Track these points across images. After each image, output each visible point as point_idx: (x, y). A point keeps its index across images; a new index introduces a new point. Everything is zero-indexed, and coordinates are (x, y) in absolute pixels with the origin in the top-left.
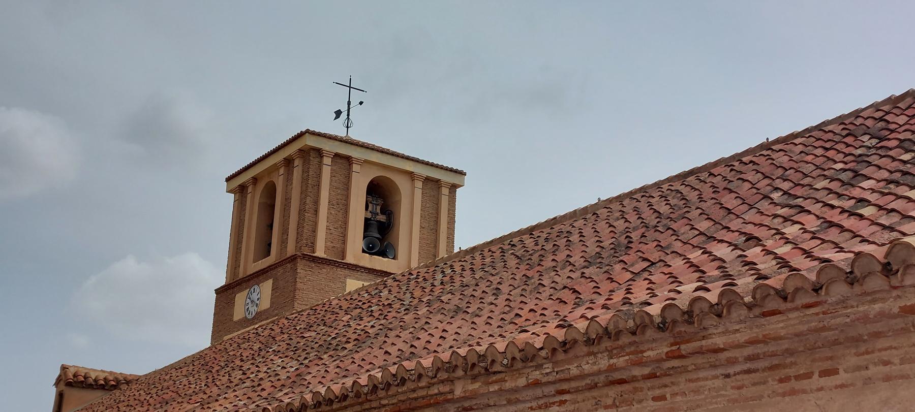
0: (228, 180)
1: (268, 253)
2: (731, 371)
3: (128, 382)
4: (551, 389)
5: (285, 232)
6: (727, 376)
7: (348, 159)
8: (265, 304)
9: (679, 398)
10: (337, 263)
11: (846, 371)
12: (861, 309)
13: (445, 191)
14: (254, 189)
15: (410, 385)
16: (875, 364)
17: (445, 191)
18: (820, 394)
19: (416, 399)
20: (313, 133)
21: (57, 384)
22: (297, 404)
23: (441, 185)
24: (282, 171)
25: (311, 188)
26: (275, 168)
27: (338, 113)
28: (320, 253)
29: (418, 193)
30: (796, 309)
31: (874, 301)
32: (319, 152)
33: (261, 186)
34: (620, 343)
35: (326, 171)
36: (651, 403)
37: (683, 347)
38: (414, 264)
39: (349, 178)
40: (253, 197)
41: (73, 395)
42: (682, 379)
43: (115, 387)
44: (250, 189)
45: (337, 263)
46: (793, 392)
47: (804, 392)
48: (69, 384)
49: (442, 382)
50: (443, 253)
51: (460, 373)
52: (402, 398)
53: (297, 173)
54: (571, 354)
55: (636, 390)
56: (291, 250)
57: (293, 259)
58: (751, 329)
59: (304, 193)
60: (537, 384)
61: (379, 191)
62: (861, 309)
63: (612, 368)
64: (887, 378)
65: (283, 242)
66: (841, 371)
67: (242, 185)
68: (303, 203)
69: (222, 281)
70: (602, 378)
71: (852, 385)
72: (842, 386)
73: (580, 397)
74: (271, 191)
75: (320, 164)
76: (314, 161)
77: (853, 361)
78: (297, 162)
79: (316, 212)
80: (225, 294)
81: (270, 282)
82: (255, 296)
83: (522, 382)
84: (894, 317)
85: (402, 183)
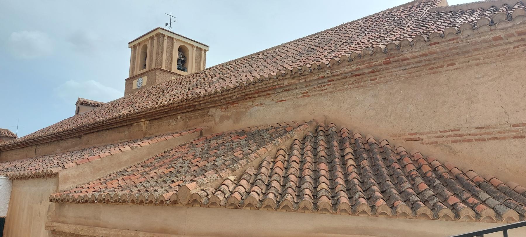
0: (129, 43)
1: (145, 68)
2: (407, 68)
3: (102, 105)
4: (326, 80)
5: (151, 61)
6: (406, 69)
7: (172, 38)
8: (145, 84)
9: (382, 79)
10: (169, 72)
11: (459, 64)
12: (474, 39)
13: (203, 52)
14: (139, 48)
15: (265, 82)
16: (472, 60)
17: (203, 52)
18: (447, 72)
19: (266, 87)
20: (161, 29)
21: (76, 104)
22: (213, 92)
23: (201, 50)
24: (150, 41)
25: (160, 47)
26: (147, 40)
27: (167, 24)
28: (164, 68)
29: (195, 52)
30: (446, 41)
31: (481, 36)
32: (163, 35)
33: (142, 46)
34: (364, 59)
35: (166, 42)
36: (370, 81)
37: (391, 59)
38: (194, 71)
39: (173, 44)
40: (139, 50)
41: (82, 108)
42: (385, 71)
43: (97, 106)
44: (137, 47)
45: (169, 72)
46: (435, 72)
47: (440, 72)
48: (82, 104)
49: (279, 80)
50: (202, 69)
51: (289, 76)
52: (260, 87)
53: (155, 42)
54: (340, 66)
55: (363, 78)
56: (153, 66)
57: (155, 69)
58: (423, 50)
59: (158, 48)
60: (323, 78)
61: (181, 50)
62: (474, 39)
63: (358, 70)
64: (478, 65)
65: (151, 64)
66: (457, 64)
67: (134, 45)
68: (157, 51)
69: (128, 77)
70: (350, 74)
71: (462, 68)
72: (457, 69)
73: (337, 82)
74: (145, 48)
75: (163, 39)
76: (161, 38)
77: (463, 60)
78: (155, 38)
79: (162, 55)
80: (129, 81)
81: (146, 77)
82: (140, 81)
83: (316, 77)
84: (490, 41)
85: (189, 48)
